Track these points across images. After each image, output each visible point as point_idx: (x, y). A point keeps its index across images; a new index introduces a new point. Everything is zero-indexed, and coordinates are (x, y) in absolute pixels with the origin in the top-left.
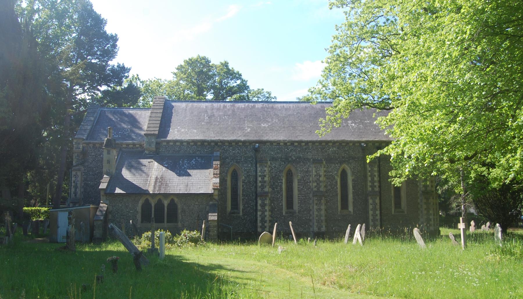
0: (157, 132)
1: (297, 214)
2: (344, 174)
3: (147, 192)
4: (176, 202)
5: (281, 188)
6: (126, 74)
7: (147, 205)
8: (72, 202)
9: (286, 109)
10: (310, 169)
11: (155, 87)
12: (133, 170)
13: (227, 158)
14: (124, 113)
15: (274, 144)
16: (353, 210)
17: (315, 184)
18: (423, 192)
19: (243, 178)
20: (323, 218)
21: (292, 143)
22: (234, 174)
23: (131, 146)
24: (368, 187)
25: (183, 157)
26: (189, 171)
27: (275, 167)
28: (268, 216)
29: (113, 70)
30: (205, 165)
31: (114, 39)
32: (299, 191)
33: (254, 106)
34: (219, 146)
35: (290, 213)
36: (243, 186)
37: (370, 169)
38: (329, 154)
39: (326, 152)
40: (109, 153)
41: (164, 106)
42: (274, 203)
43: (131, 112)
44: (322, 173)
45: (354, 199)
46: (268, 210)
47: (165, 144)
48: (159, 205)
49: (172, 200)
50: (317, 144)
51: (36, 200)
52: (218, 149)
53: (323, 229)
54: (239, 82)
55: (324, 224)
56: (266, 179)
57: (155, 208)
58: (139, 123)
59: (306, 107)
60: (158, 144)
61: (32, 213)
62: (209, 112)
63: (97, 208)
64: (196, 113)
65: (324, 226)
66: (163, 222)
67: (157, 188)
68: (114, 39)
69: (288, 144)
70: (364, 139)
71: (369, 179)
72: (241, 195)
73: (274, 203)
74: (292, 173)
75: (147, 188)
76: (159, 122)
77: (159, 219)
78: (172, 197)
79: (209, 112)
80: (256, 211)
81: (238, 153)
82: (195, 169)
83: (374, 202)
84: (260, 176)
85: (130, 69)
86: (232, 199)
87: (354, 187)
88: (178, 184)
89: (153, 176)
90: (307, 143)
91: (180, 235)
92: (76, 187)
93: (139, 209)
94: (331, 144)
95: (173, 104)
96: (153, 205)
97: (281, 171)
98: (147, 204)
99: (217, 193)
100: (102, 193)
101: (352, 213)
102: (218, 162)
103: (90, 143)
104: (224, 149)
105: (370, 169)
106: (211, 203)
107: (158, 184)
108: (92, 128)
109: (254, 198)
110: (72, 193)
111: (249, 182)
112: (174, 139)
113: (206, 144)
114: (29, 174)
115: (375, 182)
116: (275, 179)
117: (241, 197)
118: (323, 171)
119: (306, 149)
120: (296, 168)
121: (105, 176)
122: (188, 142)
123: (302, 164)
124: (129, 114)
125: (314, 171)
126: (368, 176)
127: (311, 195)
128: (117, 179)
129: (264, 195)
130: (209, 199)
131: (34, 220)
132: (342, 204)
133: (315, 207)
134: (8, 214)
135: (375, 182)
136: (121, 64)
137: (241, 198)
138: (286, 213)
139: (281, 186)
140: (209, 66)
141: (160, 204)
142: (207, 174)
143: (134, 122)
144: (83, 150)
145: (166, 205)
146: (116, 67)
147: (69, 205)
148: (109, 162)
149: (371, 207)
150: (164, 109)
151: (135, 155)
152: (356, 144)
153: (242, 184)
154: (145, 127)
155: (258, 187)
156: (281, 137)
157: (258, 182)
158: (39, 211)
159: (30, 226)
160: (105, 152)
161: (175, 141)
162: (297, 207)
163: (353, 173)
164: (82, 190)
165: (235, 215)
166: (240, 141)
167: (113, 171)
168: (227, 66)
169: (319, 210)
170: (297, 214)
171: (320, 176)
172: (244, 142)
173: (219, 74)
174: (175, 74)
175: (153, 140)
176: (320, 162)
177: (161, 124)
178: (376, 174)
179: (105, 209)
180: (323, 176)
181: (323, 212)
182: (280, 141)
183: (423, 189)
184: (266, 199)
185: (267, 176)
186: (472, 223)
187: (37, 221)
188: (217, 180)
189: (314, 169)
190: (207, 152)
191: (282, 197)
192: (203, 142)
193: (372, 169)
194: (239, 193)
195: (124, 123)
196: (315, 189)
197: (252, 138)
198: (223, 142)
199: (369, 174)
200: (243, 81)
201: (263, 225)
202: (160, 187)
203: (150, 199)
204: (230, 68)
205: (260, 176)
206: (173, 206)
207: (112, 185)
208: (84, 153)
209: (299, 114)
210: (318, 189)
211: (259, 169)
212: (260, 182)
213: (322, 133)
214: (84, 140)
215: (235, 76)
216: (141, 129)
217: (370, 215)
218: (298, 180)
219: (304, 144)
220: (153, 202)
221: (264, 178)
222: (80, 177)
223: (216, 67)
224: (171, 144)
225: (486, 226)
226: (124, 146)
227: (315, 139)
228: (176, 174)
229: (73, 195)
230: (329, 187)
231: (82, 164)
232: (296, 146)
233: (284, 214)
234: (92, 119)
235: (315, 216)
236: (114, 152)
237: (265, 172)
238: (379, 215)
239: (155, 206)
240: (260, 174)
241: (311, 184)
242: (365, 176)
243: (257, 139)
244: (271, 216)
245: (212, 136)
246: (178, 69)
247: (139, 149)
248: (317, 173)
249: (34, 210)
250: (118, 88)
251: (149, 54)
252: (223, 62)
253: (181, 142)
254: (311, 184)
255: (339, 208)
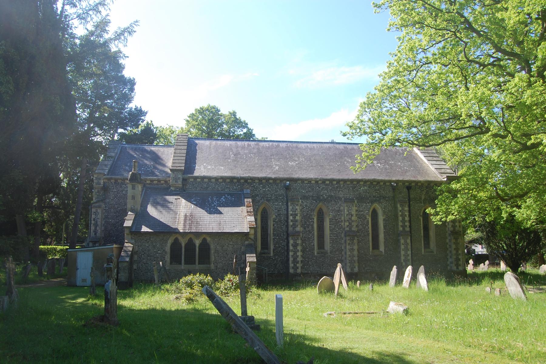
0: (183, 168)
1: (329, 254)
2: (374, 214)
3: (177, 231)
4: (208, 241)
5: (313, 227)
6: (143, 118)
7: (176, 245)
8: (92, 242)
9: (311, 149)
10: (342, 208)
11: (168, 133)
12: (159, 207)
13: (258, 195)
14: (145, 149)
15: (306, 182)
16: (385, 250)
17: (347, 224)
18: (451, 232)
19: (274, 216)
20: (356, 258)
21: (324, 181)
22: (264, 213)
23: (155, 182)
24: (400, 227)
25: (215, 194)
26: (219, 208)
27: (306, 206)
28: (300, 257)
29: (131, 113)
30: (237, 203)
31: (131, 83)
32: (330, 230)
33: (278, 146)
34: (248, 183)
35: (322, 253)
36: (273, 225)
37: (400, 209)
38: (360, 193)
39: (358, 191)
40: (133, 188)
41: (188, 143)
42: (305, 243)
43: (153, 149)
44: (354, 212)
45: (385, 239)
46: (300, 250)
47: (192, 180)
48: (190, 244)
49: (205, 240)
50: (348, 183)
51: (52, 239)
52: (247, 186)
53: (356, 270)
54: (245, 130)
55: (356, 265)
56: (298, 218)
57: (185, 248)
58: (162, 159)
59: (330, 148)
60: (184, 180)
61: (48, 251)
62: (234, 150)
63: (122, 248)
64: (220, 151)
65: (357, 267)
66: (195, 263)
67: (188, 227)
68: (131, 83)
69: (320, 182)
70: (394, 179)
71: (400, 218)
72: (272, 235)
73: (305, 243)
74: (323, 212)
75: (176, 227)
76: (184, 158)
77: (190, 260)
78: (204, 236)
79: (234, 150)
80: (288, 251)
81: (269, 191)
82: (226, 207)
83: (406, 242)
84: (291, 215)
85: (146, 113)
86: (262, 238)
87: (385, 227)
88: (209, 223)
89: (180, 214)
90: (338, 181)
91: (223, 279)
92: (96, 225)
93: (168, 248)
94: (362, 183)
95: (197, 141)
96: (183, 245)
97: (313, 210)
98: (176, 245)
99: (253, 232)
100: (126, 232)
101: (383, 253)
102: (250, 200)
103: (112, 178)
104: (254, 186)
105: (400, 209)
106: (247, 242)
107: (188, 222)
108: (113, 164)
109: (285, 237)
110: (92, 231)
111: (280, 221)
112: (202, 175)
113: (235, 181)
114: (45, 214)
115: (406, 221)
116: (307, 218)
117: (271, 237)
118: (355, 211)
119: (337, 187)
120: (328, 207)
121: (129, 213)
122: (217, 179)
123: (333, 202)
124: (151, 150)
125: (346, 211)
126: (399, 215)
127: (343, 235)
128: (142, 217)
129: (296, 234)
130: (244, 238)
131: (50, 258)
132: (373, 245)
133: (348, 247)
134: (10, 259)
135: (406, 221)
136: (139, 107)
137: (272, 237)
138: (318, 253)
139: (312, 226)
140: (219, 115)
141: (190, 244)
142: (240, 212)
143: (156, 159)
144: (104, 186)
145: (197, 245)
146: (133, 110)
147: (88, 244)
148: (133, 198)
149: (402, 247)
150: (188, 146)
151: (160, 189)
152: (387, 184)
153: (272, 223)
154: (170, 164)
155: (290, 226)
156: (311, 175)
157: (290, 221)
158: (55, 249)
159: (45, 266)
160: (130, 186)
161: (203, 178)
162: (329, 247)
163: (384, 212)
164: (103, 228)
165: (265, 255)
166: (270, 179)
167: (138, 207)
168: (235, 115)
169: (352, 250)
170: (329, 254)
171: (352, 215)
172: (275, 180)
173: (227, 123)
174: (188, 121)
175: (180, 176)
176: (351, 201)
177: (186, 160)
178: (407, 214)
179: (131, 249)
180: (355, 215)
181: (356, 253)
182: (312, 179)
183: (452, 229)
184: (298, 239)
185: (299, 215)
186: (471, 262)
187: (52, 259)
188: (252, 219)
189: (346, 208)
190: (236, 189)
191: (314, 237)
192: (232, 179)
193: (403, 209)
194: (269, 232)
195: (146, 160)
196: (347, 229)
197: (282, 175)
198: (253, 179)
199: (400, 213)
200: (249, 129)
201: (295, 265)
202: (190, 225)
203: (180, 238)
204: (238, 117)
205: (291, 215)
206: (205, 246)
207: (137, 222)
208: (105, 189)
209: (324, 154)
210: (350, 229)
211: (290, 208)
212: (292, 221)
213: (355, 171)
214: (105, 175)
215: (242, 125)
216: (164, 165)
217: (402, 255)
218: (330, 219)
219: (335, 182)
220: (183, 242)
221: (295, 217)
222: (100, 214)
223: (224, 116)
224: (199, 180)
225: (484, 265)
226: (148, 182)
227: (346, 177)
228: (206, 211)
229: (93, 234)
230: (361, 227)
231: (103, 201)
232: (327, 185)
233: (316, 254)
234: (113, 154)
235: (348, 256)
236: (139, 187)
237: (296, 210)
238: (410, 255)
239: (199, 246)
240: (291, 212)
241: (342, 224)
242: (396, 216)
243: (288, 176)
244: (302, 256)
245: (240, 172)
246: (189, 117)
247: (165, 185)
248: (349, 212)
249: (50, 248)
250: (135, 130)
251: (164, 102)
252: (231, 111)
253: (210, 178)
254: (342, 224)
255: (371, 249)
